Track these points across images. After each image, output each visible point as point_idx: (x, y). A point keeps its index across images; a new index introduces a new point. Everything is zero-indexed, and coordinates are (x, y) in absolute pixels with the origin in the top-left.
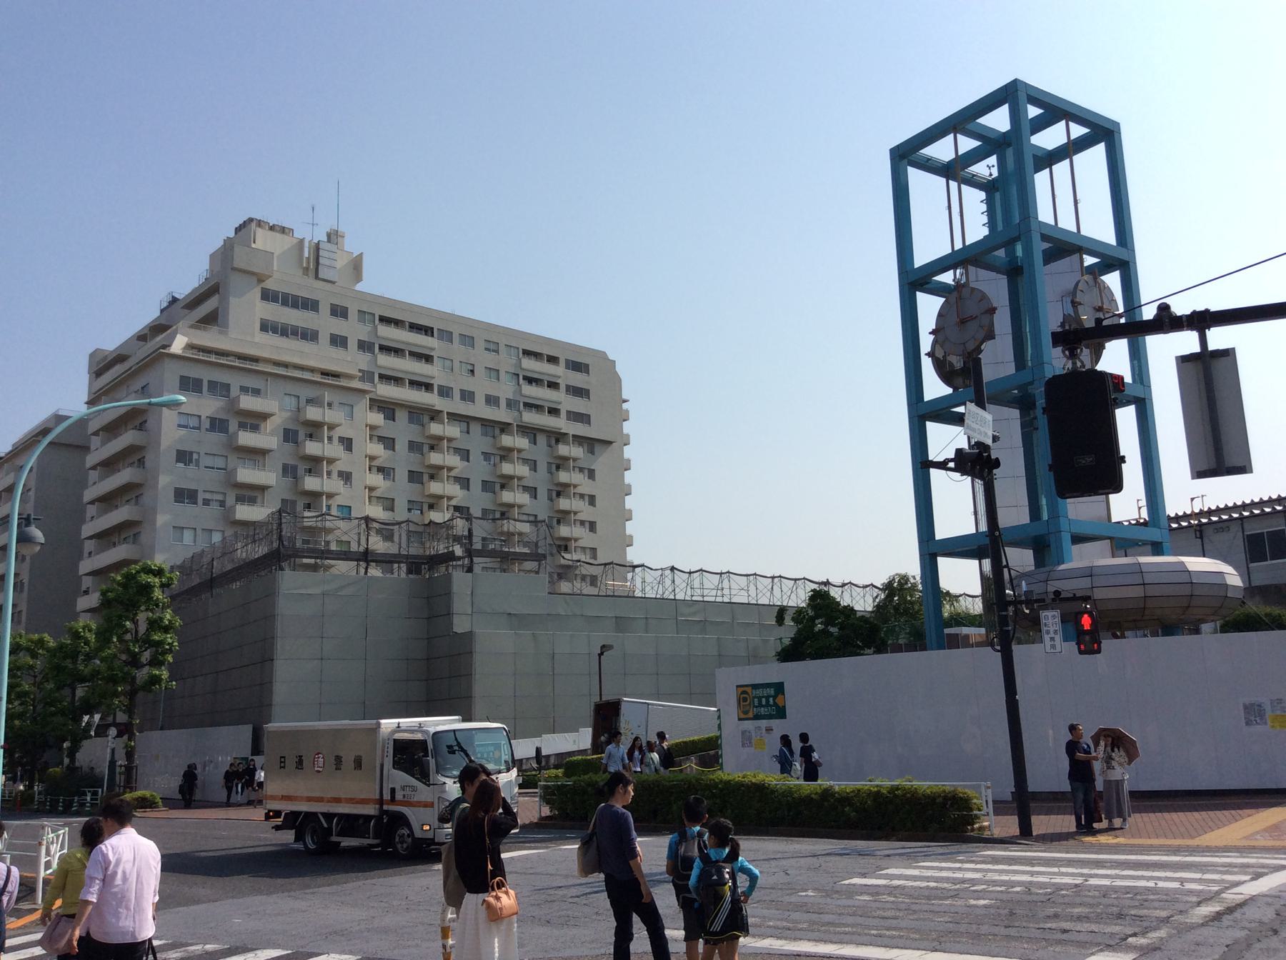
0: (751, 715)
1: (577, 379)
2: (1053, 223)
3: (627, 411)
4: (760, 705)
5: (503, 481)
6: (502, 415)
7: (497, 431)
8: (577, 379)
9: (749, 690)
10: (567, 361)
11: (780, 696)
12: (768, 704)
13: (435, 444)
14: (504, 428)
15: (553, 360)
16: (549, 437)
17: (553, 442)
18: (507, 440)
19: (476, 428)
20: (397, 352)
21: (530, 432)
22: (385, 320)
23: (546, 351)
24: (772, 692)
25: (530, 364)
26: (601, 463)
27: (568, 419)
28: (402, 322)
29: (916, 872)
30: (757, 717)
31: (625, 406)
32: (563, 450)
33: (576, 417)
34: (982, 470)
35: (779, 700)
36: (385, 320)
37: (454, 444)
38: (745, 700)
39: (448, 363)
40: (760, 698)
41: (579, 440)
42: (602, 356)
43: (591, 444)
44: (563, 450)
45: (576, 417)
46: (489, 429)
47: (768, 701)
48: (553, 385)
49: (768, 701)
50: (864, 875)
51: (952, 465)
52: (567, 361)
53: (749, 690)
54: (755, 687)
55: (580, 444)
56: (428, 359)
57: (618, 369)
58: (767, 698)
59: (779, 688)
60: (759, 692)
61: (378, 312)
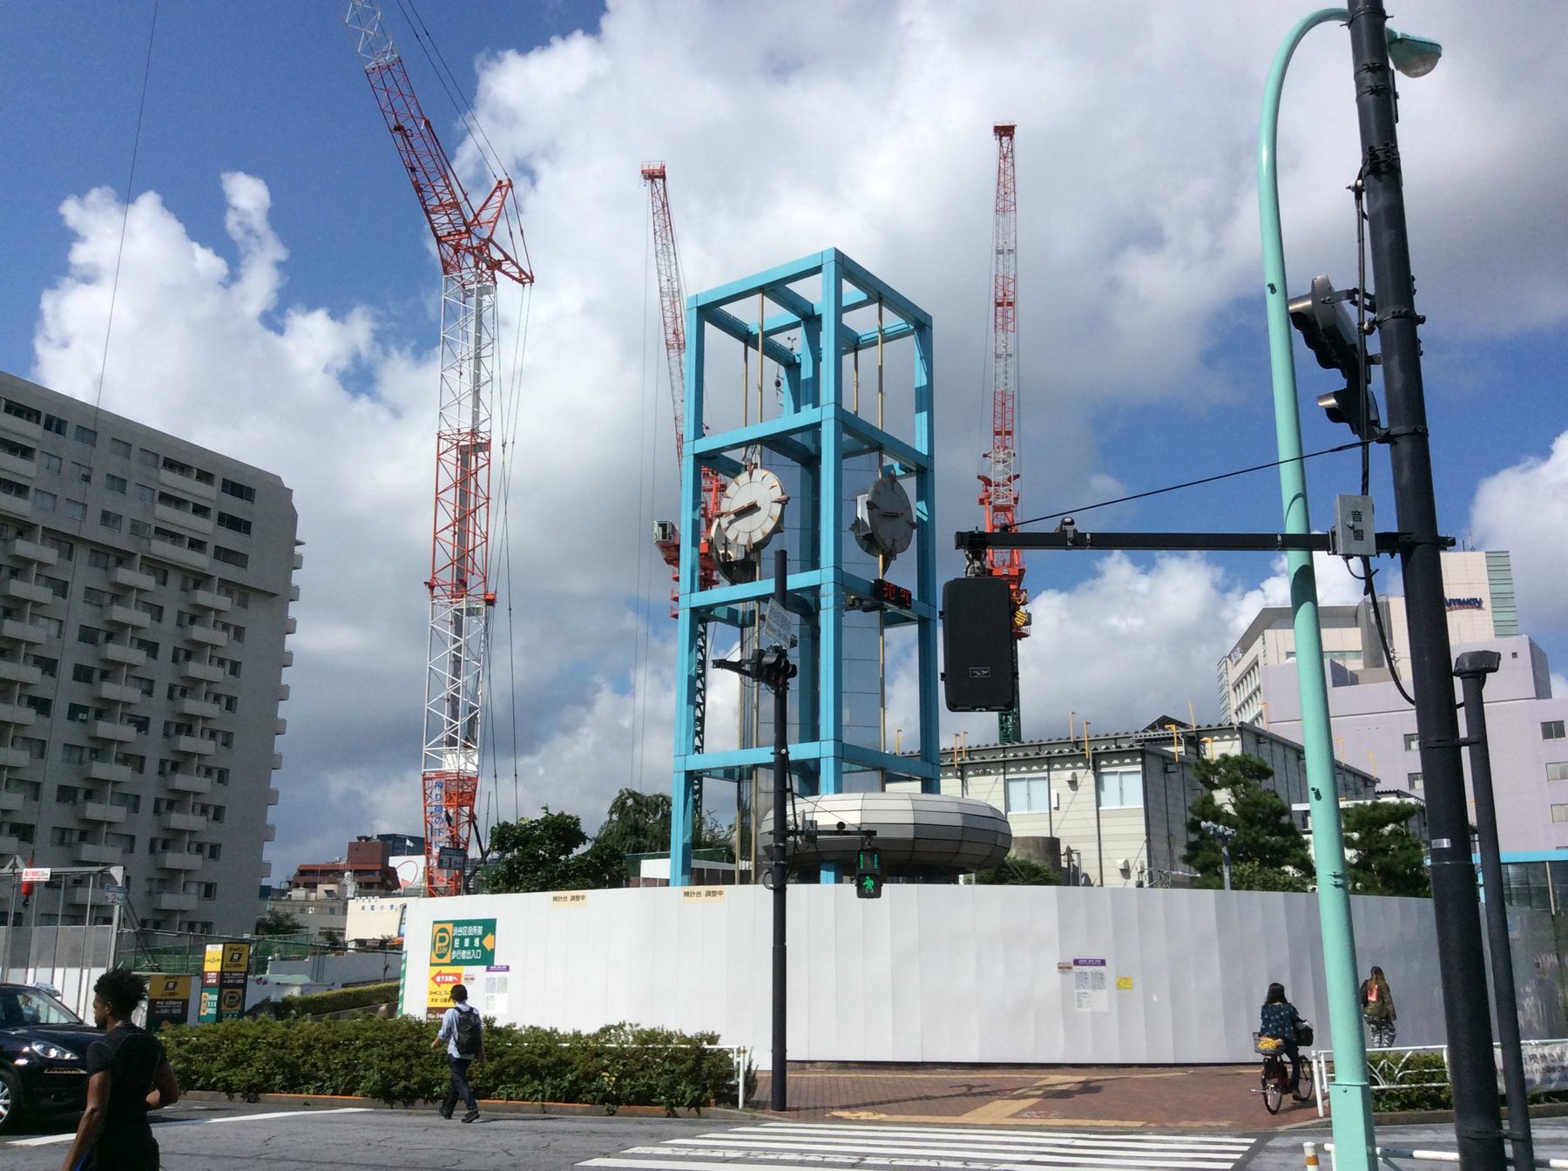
0: (447, 959)
1: (235, 506)
2: (925, 452)
3: (300, 557)
4: (462, 947)
5: (111, 629)
6: (120, 539)
7: (112, 561)
8: (235, 506)
9: (449, 927)
10: (225, 481)
11: (490, 936)
12: (472, 946)
13: (121, 593)
14: (124, 558)
15: (205, 477)
16: (186, 578)
17: (191, 584)
18: (125, 575)
19: (82, 555)
20: (178, 503)
21: (160, 569)
22: (170, 464)
23: (197, 464)
24: (479, 930)
25: (171, 479)
26: (254, 617)
27: (216, 556)
28: (190, 468)
29: (668, 1151)
30: (455, 962)
31: (298, 549)
32: (204, 597)
33: (223, 554)
34: (777, 678)
35: (488, 943)
36: (170, 464)
37: (46, 572)
38: (442, 939)
39: (55, 462)
40: (462, 939)
41: (227, 587)
42: (274, 482)
43: (243, 593)
44: (204, 597)
45: (223, 554)
46: (102, 558)
47: (472, 942)
48: (200, 510)
49: (472, 942)
50: (606, 1155)
51: (747, 667)
52: (225, 481)
53: (449, 927)
54: (457, 923)
55: (229, 593)
56: (26, 452)
57: (295, 501)
58: (472, 938)
59: (489, 926)
60: (461, 931)
61: (164, 454)
